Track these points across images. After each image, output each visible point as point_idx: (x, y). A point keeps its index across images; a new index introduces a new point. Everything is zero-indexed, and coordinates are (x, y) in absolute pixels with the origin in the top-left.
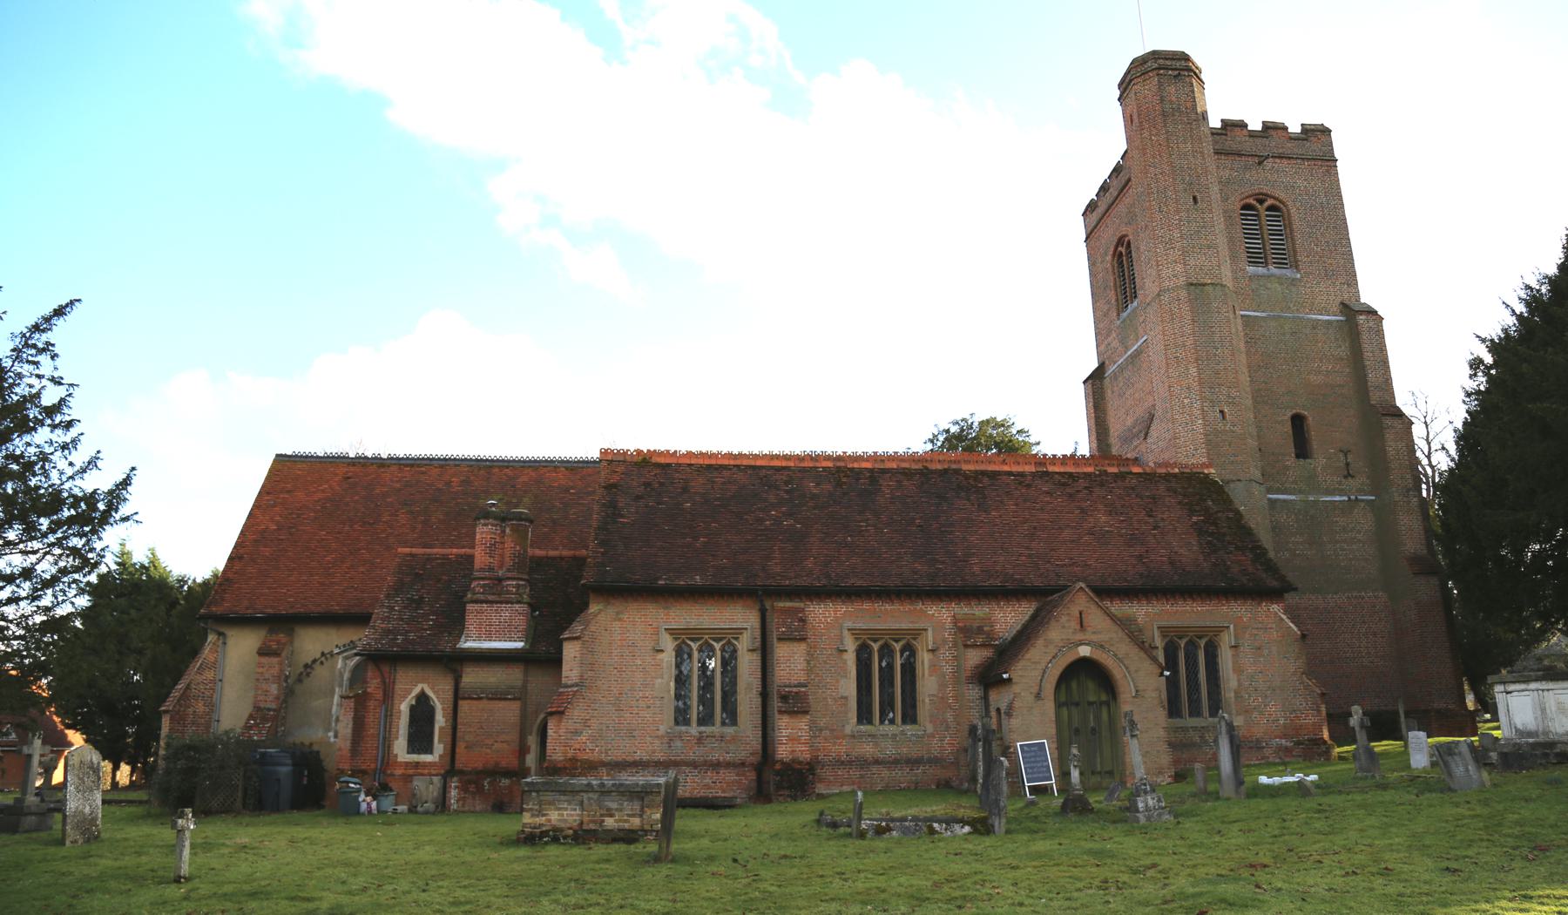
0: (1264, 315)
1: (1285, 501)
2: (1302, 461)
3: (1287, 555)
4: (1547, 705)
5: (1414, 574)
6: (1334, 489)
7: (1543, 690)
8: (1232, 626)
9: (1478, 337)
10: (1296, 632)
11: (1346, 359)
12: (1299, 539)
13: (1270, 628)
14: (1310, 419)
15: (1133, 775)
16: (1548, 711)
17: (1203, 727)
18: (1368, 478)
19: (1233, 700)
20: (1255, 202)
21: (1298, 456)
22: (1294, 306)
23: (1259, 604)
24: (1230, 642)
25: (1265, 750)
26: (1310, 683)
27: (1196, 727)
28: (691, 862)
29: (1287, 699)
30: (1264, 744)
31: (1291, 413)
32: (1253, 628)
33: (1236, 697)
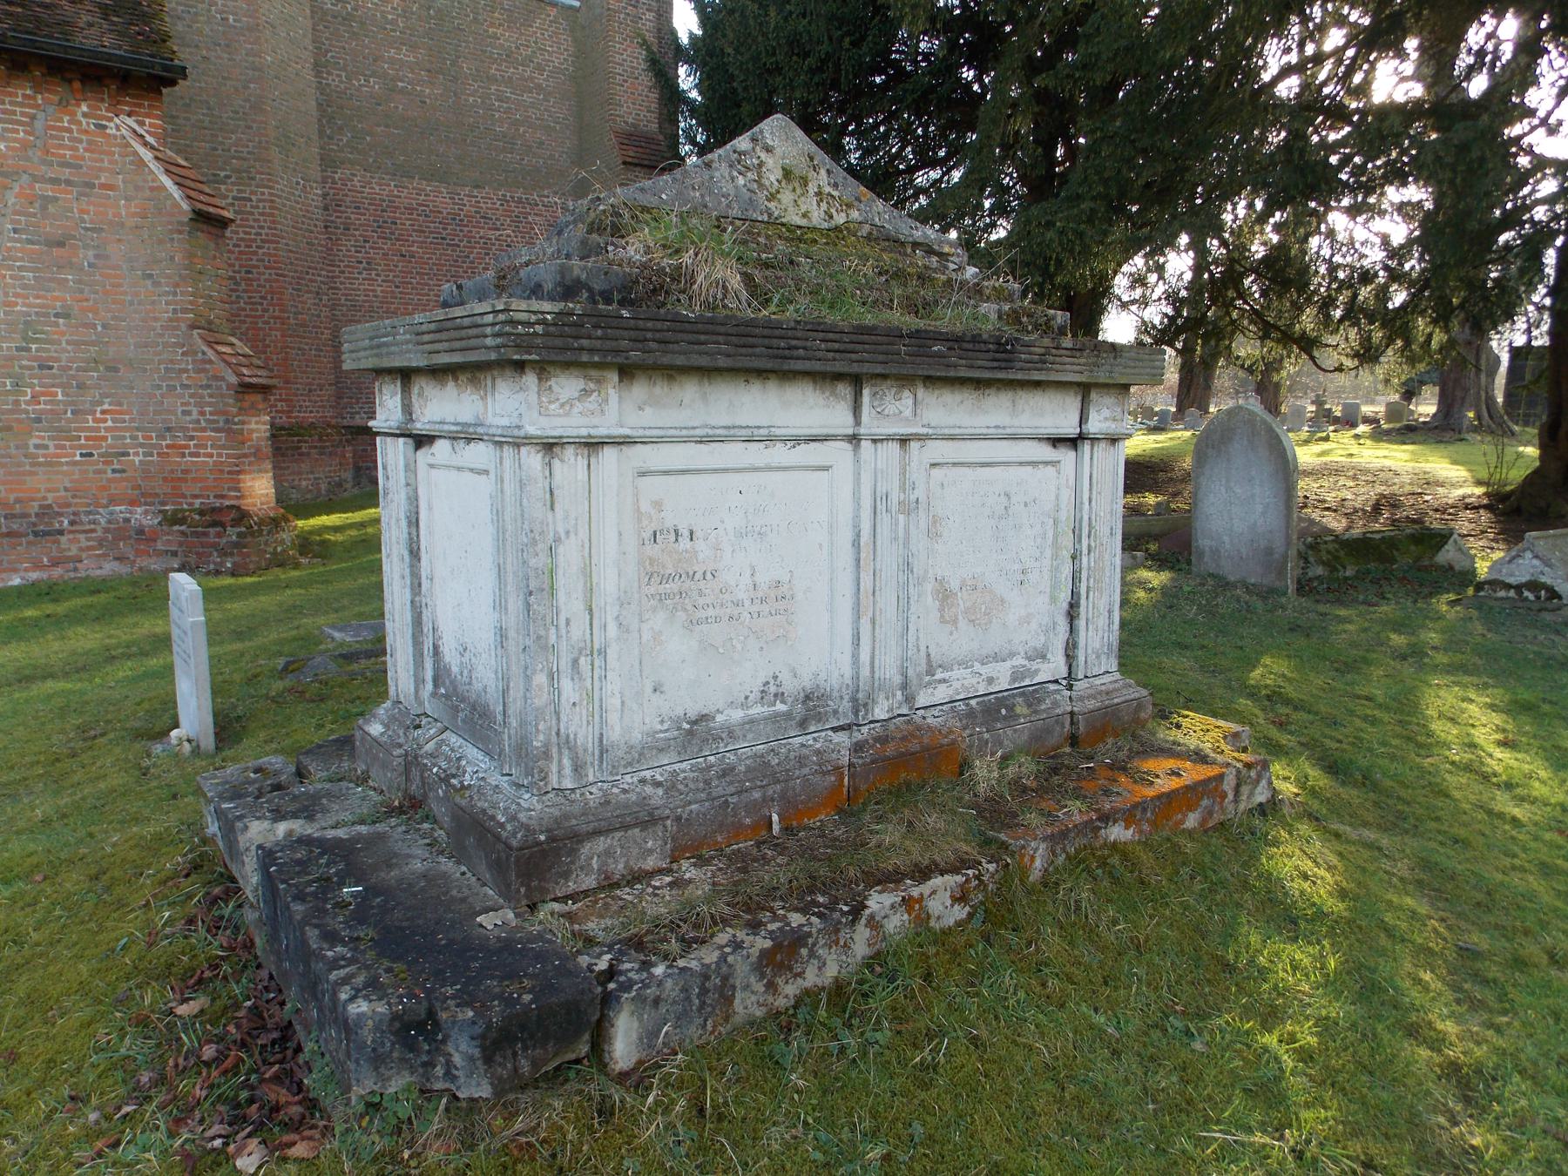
4: (570, 556)
5: (624, 163)
7: (550, 447)
10: (176, 205)
12: (405, 55)
16: (570, 602)
23: (63, 105)
25: (63, 539)
26: (211, 354)
28: (1236, 255)
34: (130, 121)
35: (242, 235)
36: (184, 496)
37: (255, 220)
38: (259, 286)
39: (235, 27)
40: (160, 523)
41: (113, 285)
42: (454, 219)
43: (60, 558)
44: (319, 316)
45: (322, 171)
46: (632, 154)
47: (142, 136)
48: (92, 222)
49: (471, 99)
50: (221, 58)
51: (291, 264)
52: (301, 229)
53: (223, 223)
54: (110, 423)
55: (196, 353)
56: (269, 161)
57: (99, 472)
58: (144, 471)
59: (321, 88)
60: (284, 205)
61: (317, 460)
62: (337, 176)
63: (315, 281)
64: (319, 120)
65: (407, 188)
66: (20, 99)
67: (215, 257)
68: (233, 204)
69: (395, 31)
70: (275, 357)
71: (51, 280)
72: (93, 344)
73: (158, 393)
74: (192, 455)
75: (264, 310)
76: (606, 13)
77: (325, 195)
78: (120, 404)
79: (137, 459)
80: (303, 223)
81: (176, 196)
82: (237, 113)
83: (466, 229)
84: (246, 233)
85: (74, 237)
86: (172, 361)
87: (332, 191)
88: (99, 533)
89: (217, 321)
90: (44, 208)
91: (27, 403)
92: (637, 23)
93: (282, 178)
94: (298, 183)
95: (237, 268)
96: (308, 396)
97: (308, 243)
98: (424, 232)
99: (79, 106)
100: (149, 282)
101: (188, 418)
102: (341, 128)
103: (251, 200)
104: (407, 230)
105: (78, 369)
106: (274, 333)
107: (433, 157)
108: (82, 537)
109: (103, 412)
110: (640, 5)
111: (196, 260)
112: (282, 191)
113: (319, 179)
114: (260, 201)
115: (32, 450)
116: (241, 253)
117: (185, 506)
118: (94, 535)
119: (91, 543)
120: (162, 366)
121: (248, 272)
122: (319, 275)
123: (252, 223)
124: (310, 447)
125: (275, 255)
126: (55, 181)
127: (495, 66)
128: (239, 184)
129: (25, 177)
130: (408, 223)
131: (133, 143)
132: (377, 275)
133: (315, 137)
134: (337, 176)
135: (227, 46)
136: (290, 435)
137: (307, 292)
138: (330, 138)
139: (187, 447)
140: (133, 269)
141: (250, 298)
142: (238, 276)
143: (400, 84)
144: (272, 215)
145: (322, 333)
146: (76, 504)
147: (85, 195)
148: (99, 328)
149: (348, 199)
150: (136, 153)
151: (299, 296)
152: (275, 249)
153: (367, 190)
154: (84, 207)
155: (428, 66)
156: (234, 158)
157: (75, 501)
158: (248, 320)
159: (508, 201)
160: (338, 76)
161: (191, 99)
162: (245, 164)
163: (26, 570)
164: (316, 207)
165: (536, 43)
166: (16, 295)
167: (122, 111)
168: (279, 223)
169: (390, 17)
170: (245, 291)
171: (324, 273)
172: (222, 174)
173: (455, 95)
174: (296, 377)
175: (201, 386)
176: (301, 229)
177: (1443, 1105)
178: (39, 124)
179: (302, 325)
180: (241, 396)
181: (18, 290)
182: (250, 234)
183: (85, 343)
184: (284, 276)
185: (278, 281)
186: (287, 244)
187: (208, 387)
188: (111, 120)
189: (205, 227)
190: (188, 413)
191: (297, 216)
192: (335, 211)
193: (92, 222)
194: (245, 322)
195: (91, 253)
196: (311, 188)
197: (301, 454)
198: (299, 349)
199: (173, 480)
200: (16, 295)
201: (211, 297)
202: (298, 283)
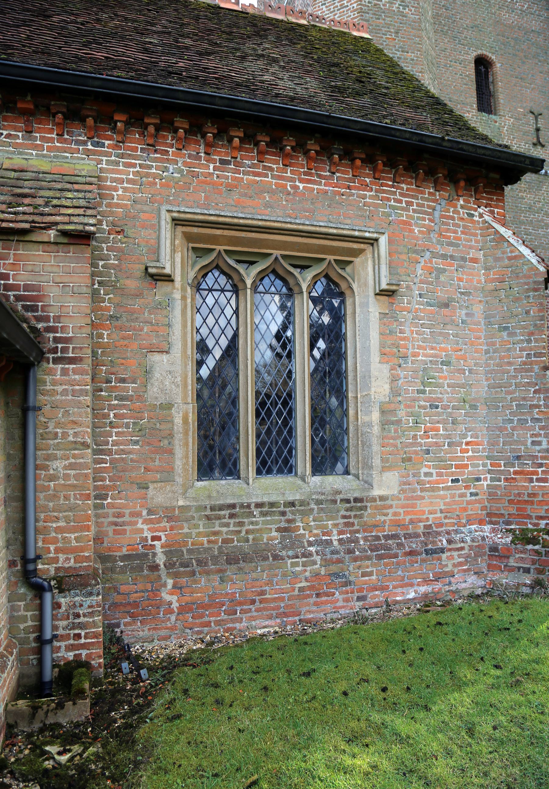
8: (383, 240)
14: (498, 65)
17: (292, 504)
19: (376, 429)
23: (450, 201)
24: (377, 279)
25: (444, 556)
27: (272, 505)
29: (501, 429)
30: (248, 28)
31: (475, 54)
32: (435, 255)
33: (384, 424)
36: (530, 517)
40: (512, 542)
43: (440, 573)
54: (470, 453)
57: (462, 495)
58: (490, 494)
66: (427, 196)
72: (462, 386)
73: (509, 426)
74: (538, 480)
79: (485, 483)
85: (453, 300)
86: (524, 399)
88: (466, 551)
90: (437, 278)
91: (422, 437)
100: (505, 334)
101: (538, 448)
105: (454, 408)
108: (455, 554)
109: (467, 444)
115: (423, 478)
117: (530, 526)
118: (463, 552)
119: (461, 560)
120: (514, 403)
126: (444, 257)
127: (523, 215)
131: (494, 224)
139: (536, 473)
146: (446, 524)
147: (461, 267)
148: (467, 373)
150: (497, 232)
157: (447, 521)
163: (418, 585)
165: (544, 199)
166: (419, 347)
178: (437, 214)
181: (421, 343)
188: (476, 210)
195: (464, 312)
199: (519, 502)
200: (419, 347)
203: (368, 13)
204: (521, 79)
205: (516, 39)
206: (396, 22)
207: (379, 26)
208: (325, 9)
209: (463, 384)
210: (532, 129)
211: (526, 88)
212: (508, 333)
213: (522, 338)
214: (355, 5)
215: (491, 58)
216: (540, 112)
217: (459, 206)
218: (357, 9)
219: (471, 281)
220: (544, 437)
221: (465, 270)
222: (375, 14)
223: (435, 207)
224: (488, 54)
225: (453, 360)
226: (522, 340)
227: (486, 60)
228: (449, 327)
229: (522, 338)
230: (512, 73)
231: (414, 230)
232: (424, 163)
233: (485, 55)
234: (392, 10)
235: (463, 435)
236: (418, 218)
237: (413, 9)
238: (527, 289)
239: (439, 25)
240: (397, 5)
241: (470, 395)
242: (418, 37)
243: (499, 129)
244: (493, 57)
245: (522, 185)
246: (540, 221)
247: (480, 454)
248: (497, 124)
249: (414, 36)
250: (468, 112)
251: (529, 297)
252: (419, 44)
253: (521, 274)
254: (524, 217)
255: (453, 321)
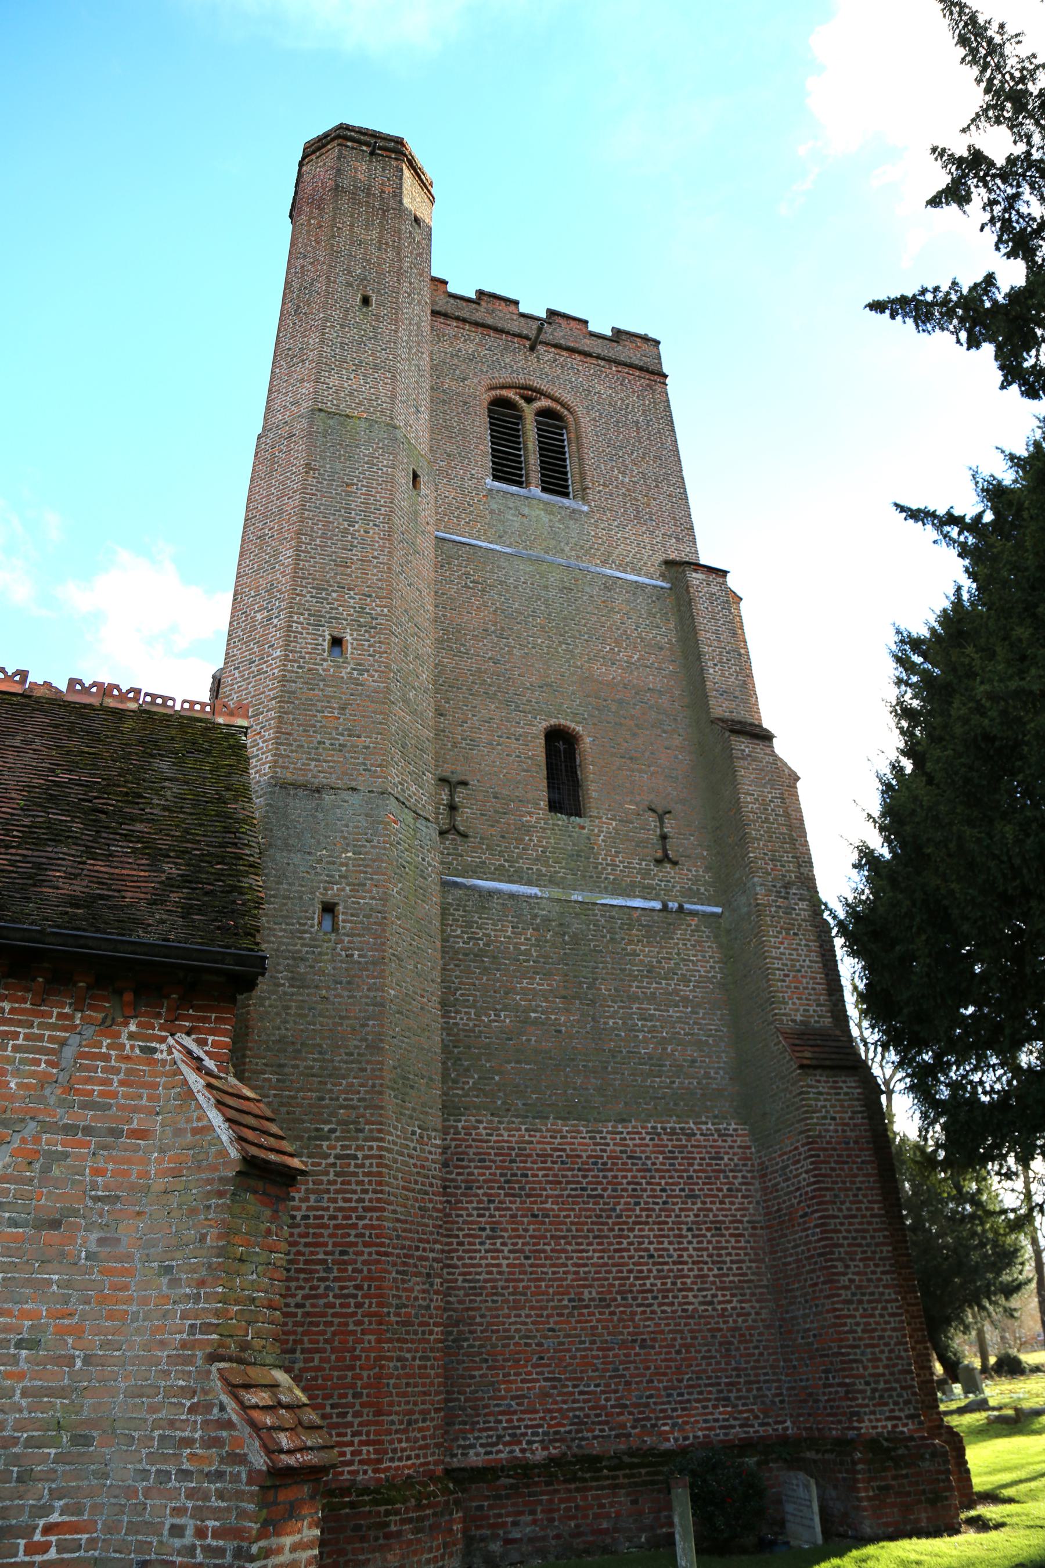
0: (508, 550)
1: (512, 896)
2: (562, 819)
3: (507, 1019)
5: (802, 1067)
6: (633, 885)
9: (916, 515)
10: (223, 1153)
11: (670, 650)
12: (540, 984)
13: (141, 1134)
14: (588, 740)
15: (1022, 1256)
18: (708, 869)
20: (517, 398)
21: (554, 806)
22: (572, 549)
23: (107, 1026)
31: (545, 724)
32: (46, 1127)
34: (189, 1042)
35: (341, 1204)
37: (358, 1183)
38: (354, 1271)
39: (359, 963)
41: (115, 1288)
42: (595, 1163)
44: (428, 1307)
45: (445, 1120)
46: (808, 1055)
47: (199, 1059)
48: (106, 1188)
49: (611, 1022)
50: (341, 996)
51: (398, 1237)
52: (413, 1191)
53: (288, 1177)
55: (208, 1407)
56: (382, 1108)
59: (447, 1029)
60: (395, 1161)
61: (410, 1542)
62: (460, 1125)
63: (426, 1259)
64: (444, 1063)
65: (540, 1131)
67: (269, 1232)
68: (334, 1165)
69: (527, 961)
70: (365, 1374)
71: (28, 1282)
72: (61, 1393)
75: (359, 1305)
76: (755, 909)
77: (446, 1148)
78: (78, 1510)
80: (416, 1182)
81: (224, 1138)
82: (352, 1054)
83: (610, 1174)
84: (345, 1200)
85: (75, 1212)
86: (172, 1424)
87: (454, 1143)
89: (257, 1343)
90: (46, 1170)
92: (791, 914)
93: (396, 1128)
94: (414, 1133)
95: (330, 1248)
96: (405, 1431)
97: (420, 1208)
98: (560, 1183)
99: (126, 1024)
100: (165, 1280)
102: (467, 1070)
103: (355, 1157)
104: (540, 1182)
105: (30, 1443)
106: (367, 1337)
107: (570, 1092)
110: (791, 896)
111: (237, 1240)
112: (395, 1143)
113: (439, 1127)
114: (366, 1157)
116: (337, 1227)
120: (156, 1433)
121: (342, 1253)
122: (432, 1250)
123: (354, 1187)
124: (403, 1522)
125: (379, 1227)
126: (69, 1129)
127: (636, 984)
128: (345, 1139)
129: (33, 1125)
130: (541, 1173)
131: (184, 1068)
132: (504, 1244)
133: (438, 1078)
134: (460, 1125)
135: (349, 983)
136: (376, 1502)
137: (416, 1275)
138: (455, 1081)
140: (148, 1258)
141: (342, 1288)
142: (330, 1258)
143: (533, 1015)
144: (380, 1174)
145: (431, 1333)
147: (105, 1148)
148: (79, 1363)
149: (471, 1151)
151: (404, 1281)
152: (378, 1219)
153: (494, 1138)
154: (101, 1164)
155: (563, 992)
156: (341, 1107)
158: (336, 1320)
159: (659, 1134)
160: (466, 1013)
161: (302, 1044)
162: (353, 1114)
164: (434, 1161)
165: (678, 954)
167: (181, 1028)
168: (388, 1184)
169: (523, 948)
170: (336, 1279)
171: (438, 1246)
172: (326, 1128)
173: (593, 1019)
174: (391, 1404)
175: (208, 1475)
176: (413, 1191)
177: (249, 1079)
178: (68, 1052)
179: (404, 1324)
180: (271, 1494)
182: (350, 1200)
183: (51, 1392)
184: (386, 1254)
185: (378, 1262)
186: (394, 1212)
187: (219, 1475)
188: (163, 1040)
189: (260, 1185)
190: (177, 1531)
191: (411, 1174)
192: (457, 1167)
193: (106, 1188)
194: (331, 1323)
195: (94, 1236)
196: (429, 1138)
197: (388, 1536)
198: (399, 1359)
201: (253, 1300)
202: (405, 1264)
203: (295, 682)
204: (631, 759)
205: (620, 702)
206: (343, 693)
207: (311, 700)
208: (237, 675)
209: (63, 1388)
210: (653, 837)
211: (640, 772)
212: (170, 1280)
213: (188, 1290)
214: (276, 671)
215: (574, 730)
216: (669, 809)
217: (124, 1035)
218: (278, 677)
219: (126, 1173)
220: (192, 1517)
221: (114, 1153)
222: (306, 683)
223: (67, 1039)
224: (568, 723)
225: (49, 1337)
226: (187, 1295)
227: (567, 733)
228: (49, 1267)
229: (188, 1290)
230: (615, 750)
231: (9, 1082)
232: (46, 965)
233: (565, 726)
234: (338, 677)
235: (43, 1507)
236: (23, 1061)
237: (376, 675)
238: (209, 1192)
239: (481, 684)
240: (349, 670)
241: (77, 1413)
242: (381, 713)
243: (589, 839)
244: (579, 729)
245: (634, 932)
246: (671, 994)
247: (82, 1553)
248: (586, 831)
249: (374, 712)
250: (530, 813)
251: (208, 1207)
252: (381, 723)
253: (205, 1163)
254: (637, 987)
255: (63, 1254)
